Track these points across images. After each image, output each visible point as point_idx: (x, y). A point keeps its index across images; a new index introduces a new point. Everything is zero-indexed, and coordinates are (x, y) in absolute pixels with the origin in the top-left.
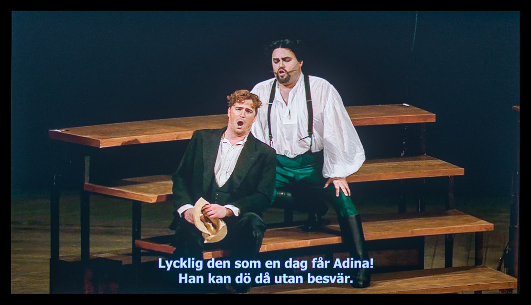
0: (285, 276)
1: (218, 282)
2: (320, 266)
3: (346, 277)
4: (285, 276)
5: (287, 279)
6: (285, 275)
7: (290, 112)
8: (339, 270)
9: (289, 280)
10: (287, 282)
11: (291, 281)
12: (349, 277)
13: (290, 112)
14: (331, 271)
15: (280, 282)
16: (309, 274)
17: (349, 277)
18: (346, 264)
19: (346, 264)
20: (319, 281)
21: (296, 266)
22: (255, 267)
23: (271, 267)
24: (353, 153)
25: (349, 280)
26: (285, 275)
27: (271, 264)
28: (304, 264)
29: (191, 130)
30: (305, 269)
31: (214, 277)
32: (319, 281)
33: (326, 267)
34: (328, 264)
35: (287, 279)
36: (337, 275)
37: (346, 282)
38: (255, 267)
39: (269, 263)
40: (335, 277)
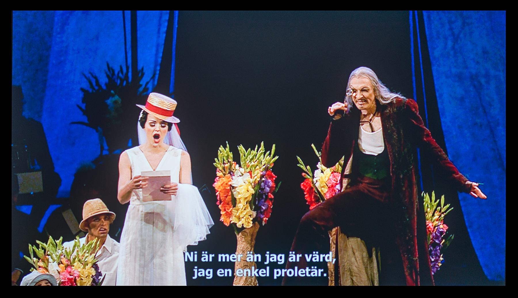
0: (308, 269)
1: (313, 275)
2: (205, 259)
3: (320, 271)
4: (308, 269)
5: (310, 273)
6: (307, 268)
7: (131, 172)
8: (311, 264)
9: (312, 274)
10: (310, 276)
11: (314, 274)
12: (322, 270)
13: (131, 172)
14: (302, 264)
15: (245, 271)
16: (30, 245)
17: (322, 270)
18: (278, 273)
19: (278, 273)
20: (302, 274)
21: (273, 259)
22: (224, 260)
23: (223, 275)
24: (87, 204)
25: (322, 273)
26: (307, 268)
27: (223, 272)
28: (209, 273)
29: (121, 190)
30: (283, 262)
31: (257, 270)
32: (302, 274)
33: (211, 260)
34: (213, 257)
35: (310, 273)
36: (313, 254)
37: (320, 275)
38: (224, 260)
39: (221, 271)
40: (311, 256)
